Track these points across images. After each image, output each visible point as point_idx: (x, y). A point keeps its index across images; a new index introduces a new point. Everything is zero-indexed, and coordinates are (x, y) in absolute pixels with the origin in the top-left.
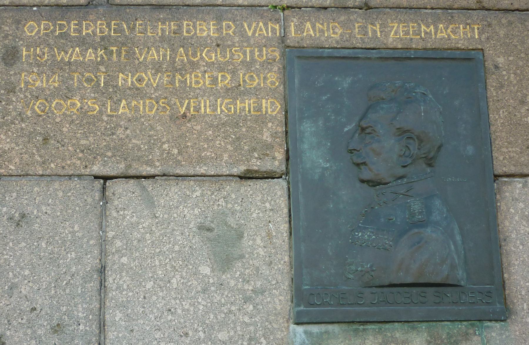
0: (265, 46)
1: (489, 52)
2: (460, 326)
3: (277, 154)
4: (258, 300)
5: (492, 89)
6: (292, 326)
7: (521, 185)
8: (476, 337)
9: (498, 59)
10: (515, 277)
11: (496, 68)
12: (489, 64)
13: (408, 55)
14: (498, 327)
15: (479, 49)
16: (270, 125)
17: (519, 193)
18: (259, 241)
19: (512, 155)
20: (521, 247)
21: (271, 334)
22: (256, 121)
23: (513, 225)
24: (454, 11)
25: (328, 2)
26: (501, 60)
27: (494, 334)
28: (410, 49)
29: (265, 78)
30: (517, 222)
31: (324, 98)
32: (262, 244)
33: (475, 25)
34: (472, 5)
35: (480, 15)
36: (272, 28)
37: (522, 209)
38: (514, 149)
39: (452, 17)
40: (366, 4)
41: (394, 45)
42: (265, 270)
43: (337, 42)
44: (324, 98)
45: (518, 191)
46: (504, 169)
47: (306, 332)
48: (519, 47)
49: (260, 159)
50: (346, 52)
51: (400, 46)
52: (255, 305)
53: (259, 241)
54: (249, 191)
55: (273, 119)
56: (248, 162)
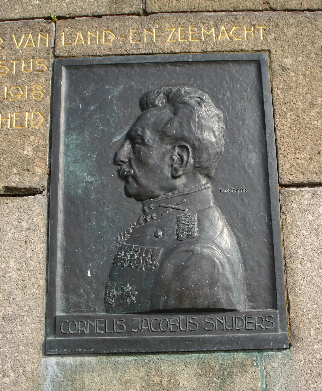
0: (33, 58)
1: (276, 53)
2: (235, 356)
3: (37, 170)
4: (7, 329)
5: (279, 92)
6: (44, 359)
7: (310, 195)
8: (254, 368)
9: (286, 60)
10: (302, 299)
11: (283, 69)
12: (276, 66)
13: (186, 59)
14: (280, 356)
15: (266, 50)
16: (32, 138)
17: (307, 204)
18: (12, 264)
19: (300, 162)
20: (309, 264)
21: (20, 367)
22: (18, 135)
23: (299, 240)
24: (239, 13)
25: (103, 10)
26: (288, 61)
27: (275, 365)
28: (189, 52)
29: (30, 90)
30: (305, 236)
31: (92, 108)
32: (16, 267)
33: (261, 26)
34: (259, 6)
35: (266, 16)
36: (41, 39)
37: (311, 221)
38: (302, 156)
39: (236, 19)
40: (144, 11)
41: (172, 49)
42: (18, 295)
43: (110, 49)
44: (92, 108)
45: (306, 202)
46: (291, 177)
47: (58, 365)
48: (309, 47)
49: (20, 174)
50: (118, 59)
51: (177, 50)
52: (4, 334)
53: (12, 264)
54: (6, 210)
55: (35, 132)
56: (7, 178)
